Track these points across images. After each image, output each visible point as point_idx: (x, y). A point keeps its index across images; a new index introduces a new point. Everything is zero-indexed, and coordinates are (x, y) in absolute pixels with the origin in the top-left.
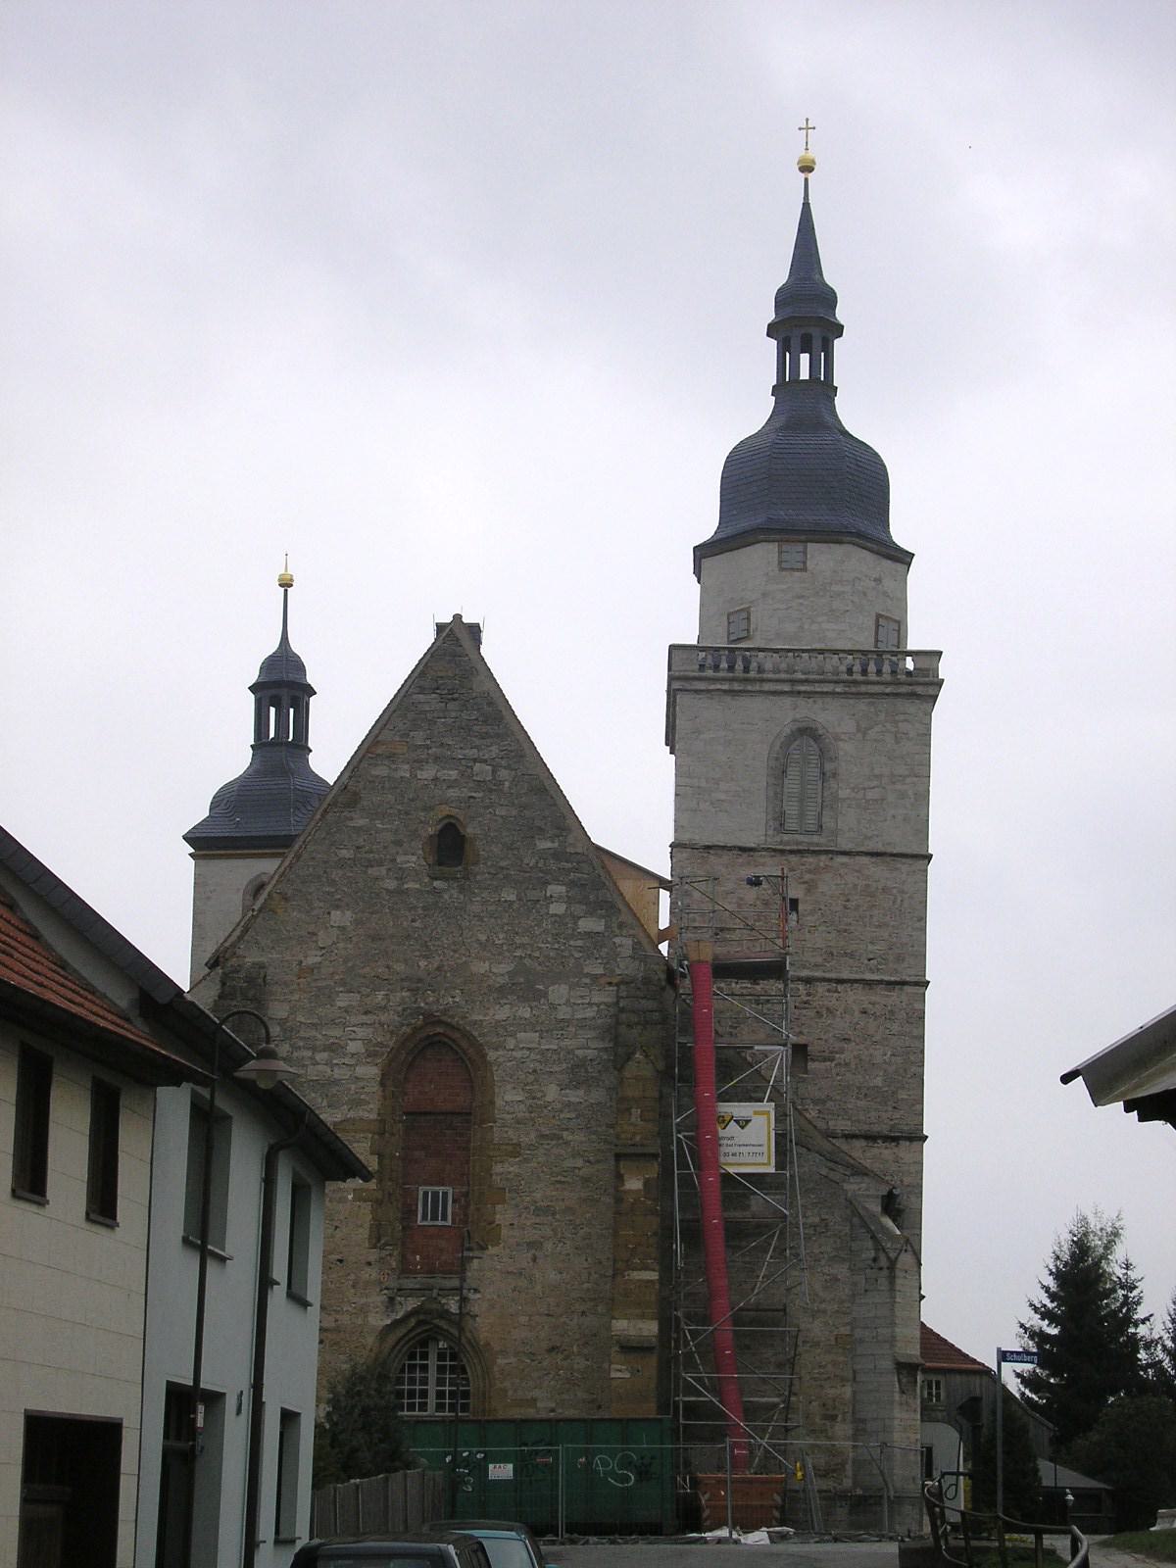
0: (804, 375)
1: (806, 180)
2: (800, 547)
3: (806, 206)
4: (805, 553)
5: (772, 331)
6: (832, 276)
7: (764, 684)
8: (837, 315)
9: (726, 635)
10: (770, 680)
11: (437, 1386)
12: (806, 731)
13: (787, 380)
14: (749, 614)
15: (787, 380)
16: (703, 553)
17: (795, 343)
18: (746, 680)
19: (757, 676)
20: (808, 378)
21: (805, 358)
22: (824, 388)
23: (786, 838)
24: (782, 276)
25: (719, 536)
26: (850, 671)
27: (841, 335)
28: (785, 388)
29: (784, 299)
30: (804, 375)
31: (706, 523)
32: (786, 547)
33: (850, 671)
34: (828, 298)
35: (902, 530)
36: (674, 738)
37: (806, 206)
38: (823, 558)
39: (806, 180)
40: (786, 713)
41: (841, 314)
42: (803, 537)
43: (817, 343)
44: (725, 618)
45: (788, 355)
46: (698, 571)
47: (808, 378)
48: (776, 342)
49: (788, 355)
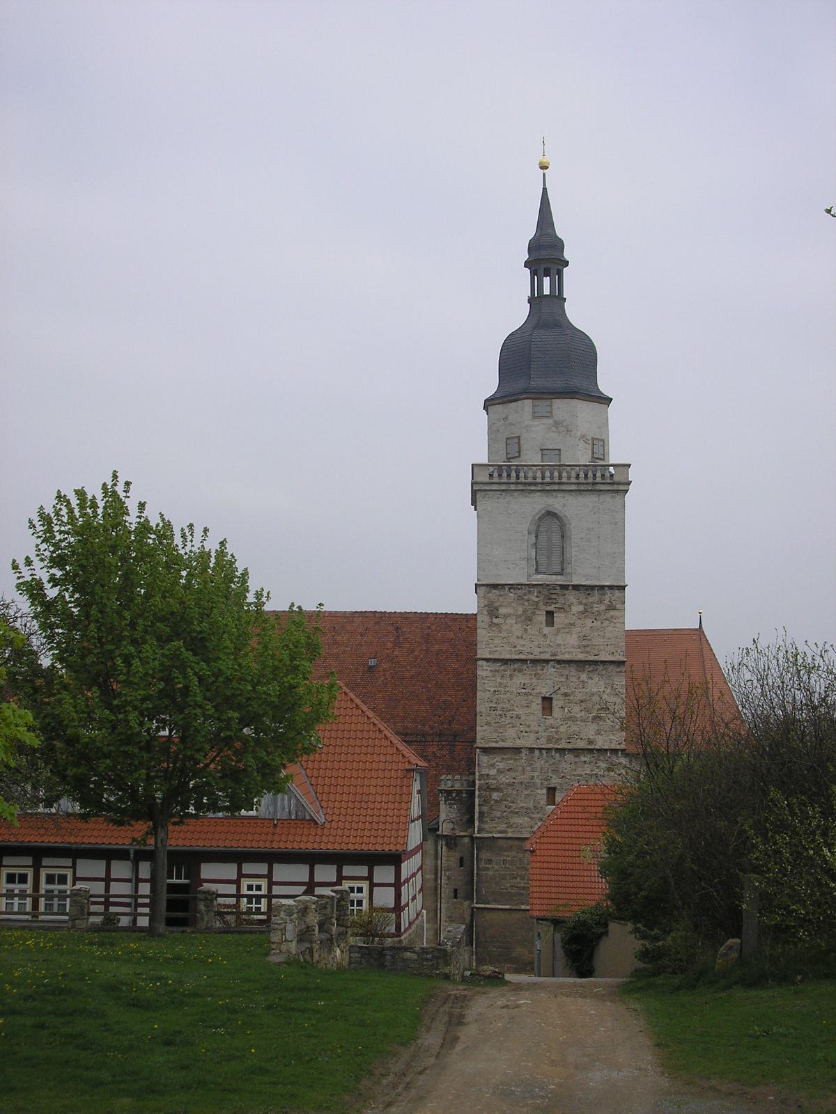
0: (547, 291)
1: (544, 174)
2: (548, 402)
3: (545, 190)
4: (551, 406)
5: (527, 265)
6: (560, 231)
7: (620, 486)
8: (565, 256)
9: (505, 454)
10: (583, 484)
11: (357, 901)
12: (550, 514)
13: (536, 296)
14: (519, 440)
15: (536, 296)
16: (489, 404)
17: (541, 272)
18: (543, 484)
19: (567, 481)
20: (549, 293)
21: (547, 280)
22: (558, 298)
23: (540, 576)
24: (531, 231)
25: (497, 395)
26: (578, 477)
27: (568, 265)
28: (536, 301)
29: (534, 246)
30: (547, 291)
31: (490, 384)
32: (537, 402)
33: (578, 477)
34: (559, 245)
35: (605, 384)
36: (476, 502)
37: (545, 190)
38: (562, 407)
39: (544, 174)
40: (535, 504)
41: (567, 255)
42: (550, 396)
43: (553, 271)
44: (503, 445)
45: (536, 277)
46: (474, 503)
47: (549, 293)
48: (529, 271)
49: (536, 277)
